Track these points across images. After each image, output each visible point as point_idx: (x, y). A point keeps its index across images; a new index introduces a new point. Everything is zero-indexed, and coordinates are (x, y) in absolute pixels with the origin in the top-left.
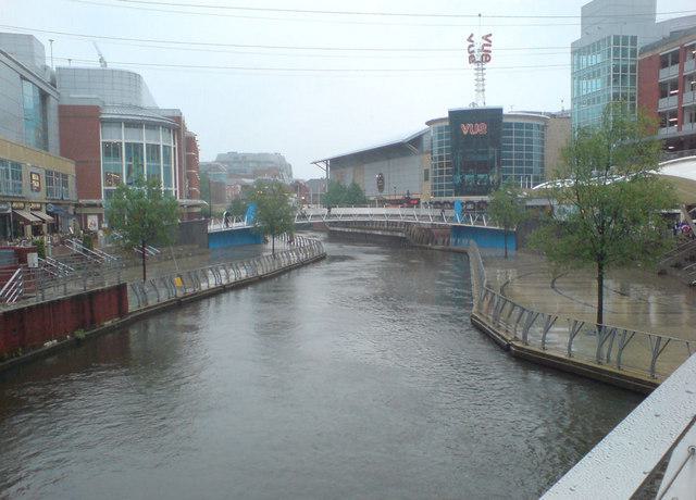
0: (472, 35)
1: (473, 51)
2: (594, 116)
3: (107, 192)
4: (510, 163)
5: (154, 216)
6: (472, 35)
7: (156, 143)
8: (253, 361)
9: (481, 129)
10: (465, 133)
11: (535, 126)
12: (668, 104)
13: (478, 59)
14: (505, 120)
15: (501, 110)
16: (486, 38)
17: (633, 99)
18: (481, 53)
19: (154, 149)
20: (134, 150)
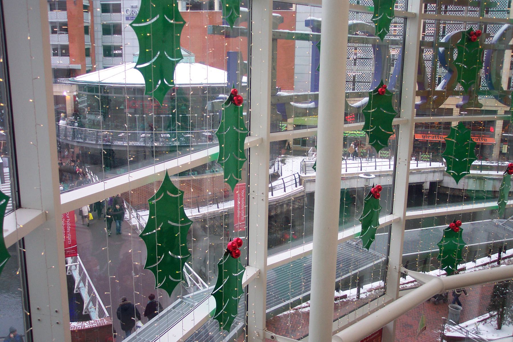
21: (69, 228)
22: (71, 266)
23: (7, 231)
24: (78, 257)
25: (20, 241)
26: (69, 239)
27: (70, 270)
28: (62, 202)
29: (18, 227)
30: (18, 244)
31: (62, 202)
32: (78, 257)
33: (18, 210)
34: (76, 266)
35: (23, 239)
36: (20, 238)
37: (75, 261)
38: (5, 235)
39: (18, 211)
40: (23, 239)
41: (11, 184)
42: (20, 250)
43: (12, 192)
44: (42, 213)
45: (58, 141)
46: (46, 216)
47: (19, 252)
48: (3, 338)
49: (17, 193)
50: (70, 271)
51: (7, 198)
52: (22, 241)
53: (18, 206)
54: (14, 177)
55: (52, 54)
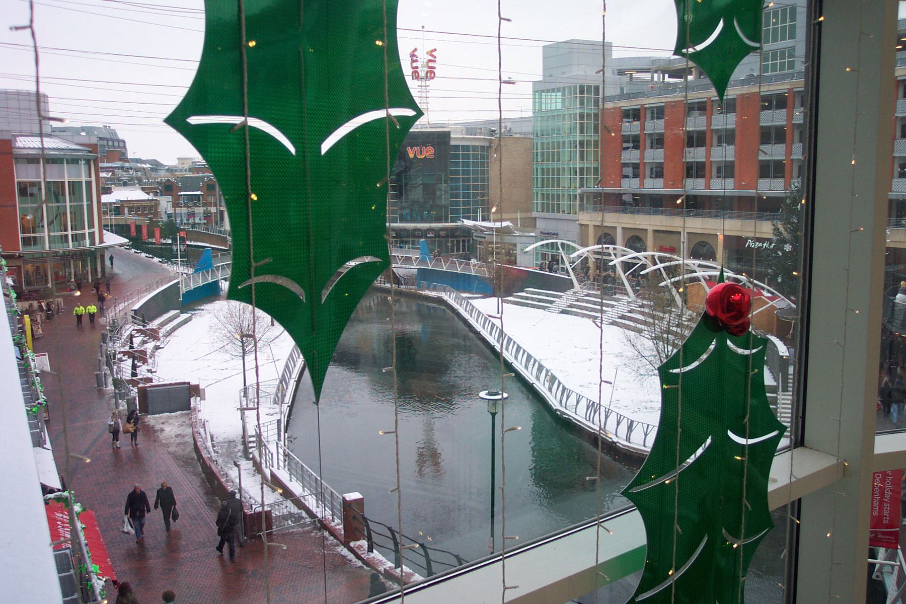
0: (416, 50)
1: (417, 67)
2: (528, 128)
3: (23, 238)
4: (457, 172)
5: (509, 125)
6: (416, 50)
7: (78, 179)
8: (134, 435)
9: (428, 152)
10: (411, 156)
11: (496, 138)
12: (696, 155)
13: (422, 74)
14: (452, 143)
15: (449, 133)
16: (431, 53)
17: (596, 145)
18: (426, 69)
19: (75, 187)
20: (56, 191)
21: (888, 494)
22: (882, 565)
23: (775, 481)
24: (900, 551)
25: (793, 503)
26: (886, 513)
27: (880, 570)
28: (877, 451)
29: (793, 479)
30: (789, 506)
31: (877, 451)
32: (900, 551)
33: (799, 449)
34: (893, 567)
35: (800, 500)
36: (795, 498)
37: (892, 557)
38: (771, 487)
39: (798, 451)
40: (800, 500)
41: (793, 401)
42: (792, 521)
43: (791, 422)
44: (838, 465)
45: (884, 330)
46: (843, 471)
47: (788, 521)
48: (262, 488)
49: (800, 420)
50: (878, 574)
51: (782, 429)
52: (796, 503)
53: (799, 442)
54: (810, 151)
55: (896, 173)
